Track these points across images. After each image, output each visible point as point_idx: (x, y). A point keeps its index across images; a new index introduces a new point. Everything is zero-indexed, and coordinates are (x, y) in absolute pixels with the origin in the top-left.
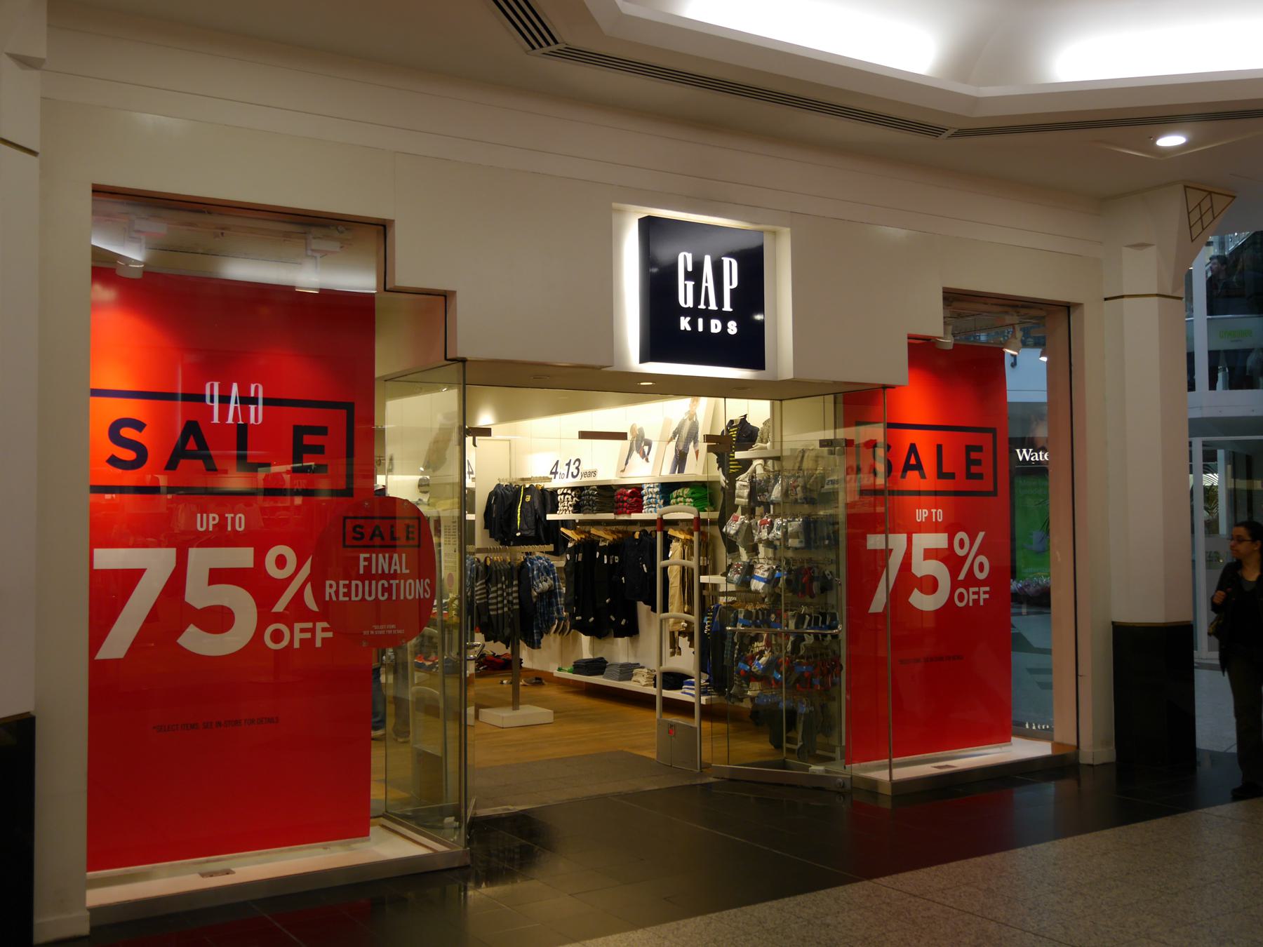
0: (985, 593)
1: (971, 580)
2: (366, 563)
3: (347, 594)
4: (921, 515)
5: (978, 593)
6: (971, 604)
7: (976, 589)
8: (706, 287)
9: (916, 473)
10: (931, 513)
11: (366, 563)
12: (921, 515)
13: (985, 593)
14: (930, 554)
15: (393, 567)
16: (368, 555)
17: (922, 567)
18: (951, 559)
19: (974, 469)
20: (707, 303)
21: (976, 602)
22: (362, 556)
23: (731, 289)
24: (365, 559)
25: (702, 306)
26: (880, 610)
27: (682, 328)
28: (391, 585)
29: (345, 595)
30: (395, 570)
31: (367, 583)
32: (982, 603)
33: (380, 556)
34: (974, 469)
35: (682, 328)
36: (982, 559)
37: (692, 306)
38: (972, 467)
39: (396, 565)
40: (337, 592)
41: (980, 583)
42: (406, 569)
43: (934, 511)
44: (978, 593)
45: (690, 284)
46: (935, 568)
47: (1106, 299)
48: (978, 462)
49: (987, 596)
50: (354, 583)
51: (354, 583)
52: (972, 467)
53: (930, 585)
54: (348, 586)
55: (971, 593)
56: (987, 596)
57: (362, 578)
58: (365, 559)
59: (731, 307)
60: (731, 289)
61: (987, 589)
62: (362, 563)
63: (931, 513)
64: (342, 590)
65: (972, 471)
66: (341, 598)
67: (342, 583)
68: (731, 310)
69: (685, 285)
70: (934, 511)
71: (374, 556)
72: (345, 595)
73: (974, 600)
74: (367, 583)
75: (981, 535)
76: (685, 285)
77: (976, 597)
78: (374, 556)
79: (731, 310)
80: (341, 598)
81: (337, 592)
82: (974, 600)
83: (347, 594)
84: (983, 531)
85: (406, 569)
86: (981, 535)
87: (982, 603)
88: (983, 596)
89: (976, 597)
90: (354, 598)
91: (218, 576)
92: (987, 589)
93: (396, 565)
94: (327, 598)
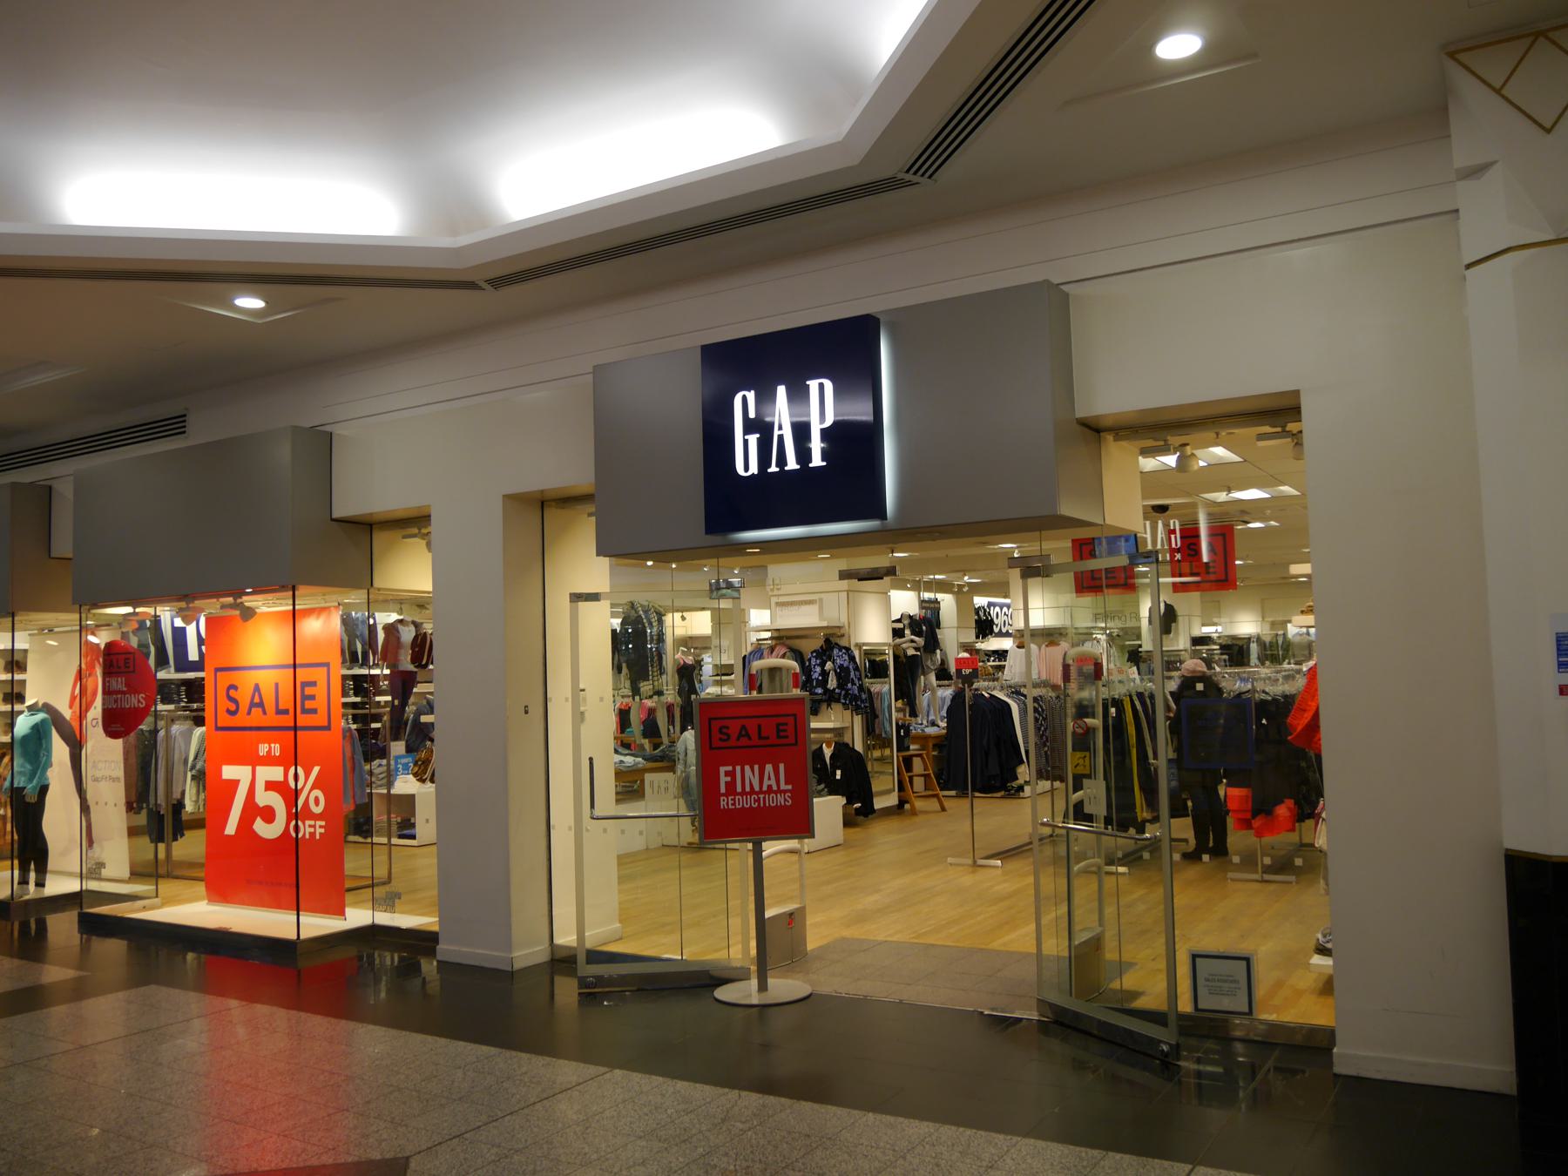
0: (321, 827)
1: (307, 814)
2: (729, 779)
3: (734, 804)
4: (263, 749)
5: (314, 826)
6: (307, 836)
7: (312, 823)
8: (781, 438)
9: (260, 710)
10: (270, 748)
11: (729, 779)
12: (263, 749)
13: (321, 827)
14: (270, 786)
15: (766, 783)
16: (730, 768)
17: (264, 798)
18: (291, 796)
19: (782, 734)
20: (782, 460)
21: (312, 835)
22: (723, 770)
23: (822, 430)
24: (727, 773)
25: (774, 469)
26: (233, 833)
27: (753, 392)
28: (759, 798)
29: (732, 804)
30: (770, 787)
31: (745, 797)
32: (318, 837)
33: (747, 768)
34: (782, 734)
35: (753, 392)
36: (318, 793)
37: (756, 473)
38: (306, 702)
39: (769, 779)
40: (727, 804)
41: (316, 817)
42: (786, 783)
43: (273, 745)
44: (314, 826)
45: (753, 439)
46: (275, 801)
47: (1468, 266)
48: (313, 697)
49: (323, 831)
50: (737, 797)
51: (737, 797)
52: (306, 702)
53: (268, 814)
54: (734, 800)
55: (307, 826)
56: (323, 831)
57: (739, 794)
58: (727, 773)
59: (798, 463)
60: (822, 430)
61: (323, 823)
62: (724, 779)
63: (270, 748)
64: (730, 802)
65: (306, 693)
66: (730, 807)
67: (730, 798)
68: (798, 467)
69: (746, 442)
70: (273, 745)
71: (738, 768)
72: (732, 804)
73: (310, 833)
74: (745, 797)
75: (316, 770)
76: (746, 442)
77: (312, 830)
78: (738, 768)
79: (798, 467)
80: (730, 807)
81: (727, 804)
82: (310, 833)
83: (734, 804)
84: (318, 765)
85: (786, 783)
86: (316, 770)
87: (318, 837)
88: (319, 831)
89: (312, 830)
90: (737, 807)
91: (270, 786)
92: (323, 823)
93: (769, 779)
94: (722, 807)
